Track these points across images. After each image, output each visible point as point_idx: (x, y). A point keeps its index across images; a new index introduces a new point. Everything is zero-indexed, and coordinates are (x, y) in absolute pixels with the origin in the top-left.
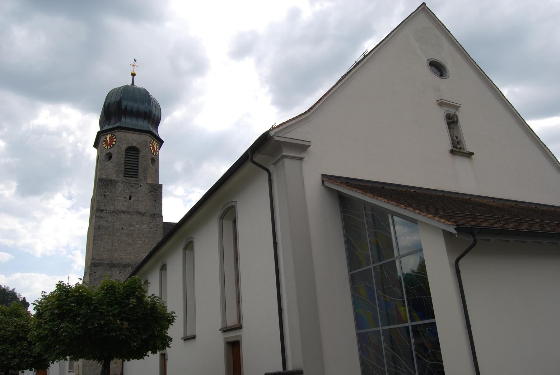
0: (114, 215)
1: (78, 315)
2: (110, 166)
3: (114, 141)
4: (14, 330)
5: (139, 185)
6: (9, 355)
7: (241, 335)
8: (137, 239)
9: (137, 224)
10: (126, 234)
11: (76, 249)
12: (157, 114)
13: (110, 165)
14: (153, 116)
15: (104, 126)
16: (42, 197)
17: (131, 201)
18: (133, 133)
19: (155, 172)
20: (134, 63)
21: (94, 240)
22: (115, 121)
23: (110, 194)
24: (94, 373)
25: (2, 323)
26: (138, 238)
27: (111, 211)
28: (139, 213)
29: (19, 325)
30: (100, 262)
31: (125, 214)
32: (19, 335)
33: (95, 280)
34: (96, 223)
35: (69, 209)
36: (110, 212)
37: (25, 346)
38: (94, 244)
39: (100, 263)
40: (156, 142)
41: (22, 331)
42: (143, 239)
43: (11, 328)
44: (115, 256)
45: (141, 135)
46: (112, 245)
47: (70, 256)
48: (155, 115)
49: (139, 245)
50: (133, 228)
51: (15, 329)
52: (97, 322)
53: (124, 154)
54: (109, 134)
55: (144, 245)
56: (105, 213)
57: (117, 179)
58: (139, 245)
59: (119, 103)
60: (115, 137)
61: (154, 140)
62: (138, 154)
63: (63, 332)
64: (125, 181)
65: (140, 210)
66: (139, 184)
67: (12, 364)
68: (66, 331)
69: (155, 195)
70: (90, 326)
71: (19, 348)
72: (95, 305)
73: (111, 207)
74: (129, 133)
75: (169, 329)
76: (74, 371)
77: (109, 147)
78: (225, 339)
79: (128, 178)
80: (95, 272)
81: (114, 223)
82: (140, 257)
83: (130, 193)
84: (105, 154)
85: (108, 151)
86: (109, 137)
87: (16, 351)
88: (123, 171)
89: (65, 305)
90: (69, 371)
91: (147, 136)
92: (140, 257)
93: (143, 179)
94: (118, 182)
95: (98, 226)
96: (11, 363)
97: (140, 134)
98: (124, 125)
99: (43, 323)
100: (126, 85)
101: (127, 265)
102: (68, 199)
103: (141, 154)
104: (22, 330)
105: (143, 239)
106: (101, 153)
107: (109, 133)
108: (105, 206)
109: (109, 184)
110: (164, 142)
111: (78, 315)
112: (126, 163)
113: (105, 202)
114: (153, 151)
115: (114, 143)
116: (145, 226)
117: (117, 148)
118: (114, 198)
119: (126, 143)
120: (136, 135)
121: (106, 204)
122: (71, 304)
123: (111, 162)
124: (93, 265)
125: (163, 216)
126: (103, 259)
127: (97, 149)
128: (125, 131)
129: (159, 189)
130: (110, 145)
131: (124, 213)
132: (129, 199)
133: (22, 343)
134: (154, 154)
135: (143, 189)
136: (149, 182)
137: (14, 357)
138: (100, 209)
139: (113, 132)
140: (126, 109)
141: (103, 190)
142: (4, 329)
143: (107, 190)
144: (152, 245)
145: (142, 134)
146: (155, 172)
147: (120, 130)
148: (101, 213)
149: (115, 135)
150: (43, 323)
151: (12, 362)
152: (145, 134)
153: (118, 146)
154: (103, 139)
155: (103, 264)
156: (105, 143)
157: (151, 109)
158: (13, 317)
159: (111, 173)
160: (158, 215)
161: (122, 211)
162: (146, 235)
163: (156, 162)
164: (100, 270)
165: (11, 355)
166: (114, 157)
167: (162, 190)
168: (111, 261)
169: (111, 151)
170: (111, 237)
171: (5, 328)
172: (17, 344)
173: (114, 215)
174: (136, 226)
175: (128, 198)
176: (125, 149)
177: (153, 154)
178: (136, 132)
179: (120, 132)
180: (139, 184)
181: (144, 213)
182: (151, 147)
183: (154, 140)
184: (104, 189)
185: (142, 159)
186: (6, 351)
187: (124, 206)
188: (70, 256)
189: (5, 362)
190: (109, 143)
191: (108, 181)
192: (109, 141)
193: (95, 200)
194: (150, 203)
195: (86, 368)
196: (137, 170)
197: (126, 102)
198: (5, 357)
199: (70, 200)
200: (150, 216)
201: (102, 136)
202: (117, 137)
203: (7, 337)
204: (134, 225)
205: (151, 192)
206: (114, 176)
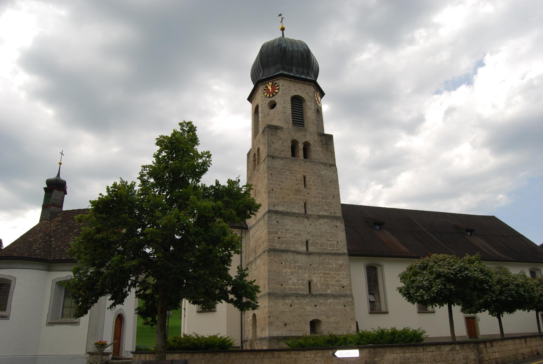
60: (277, 85)
75: (229, 271)
77: (271, 95)
78: (464, 316)
110: (325, 94)
114: (317, 102)
115: (277, 91)
130: (272, 93)
139: (275, 80)
156: (266, 91)
190: (271, 91)
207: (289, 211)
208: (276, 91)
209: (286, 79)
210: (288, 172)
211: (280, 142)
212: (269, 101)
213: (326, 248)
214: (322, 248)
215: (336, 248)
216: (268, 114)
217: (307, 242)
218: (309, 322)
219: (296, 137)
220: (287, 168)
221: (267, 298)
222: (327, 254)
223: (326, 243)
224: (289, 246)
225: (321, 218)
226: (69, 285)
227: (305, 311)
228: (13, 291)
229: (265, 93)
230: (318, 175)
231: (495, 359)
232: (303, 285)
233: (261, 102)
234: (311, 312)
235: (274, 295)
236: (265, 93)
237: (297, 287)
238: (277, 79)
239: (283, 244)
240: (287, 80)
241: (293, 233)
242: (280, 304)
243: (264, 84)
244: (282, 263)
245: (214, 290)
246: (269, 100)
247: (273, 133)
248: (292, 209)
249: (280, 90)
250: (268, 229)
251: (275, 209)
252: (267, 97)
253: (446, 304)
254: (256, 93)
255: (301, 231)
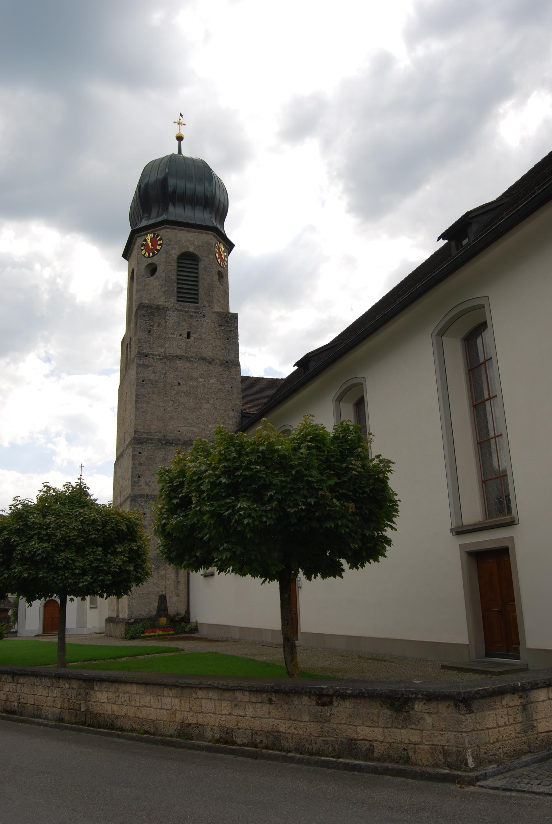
0: (165, 363)
1: (267, 487)
2: (154, 284)
3: (160, 245)
4: (81, 528)
5: (201, 315)
6: (76, 569)
7: (513, 537)
8: (203, 402)
9: (201, 377)
10: (184, 393)
11: (58, 434)
12: (222, 200)
13: (154, 282)
14: (217, 202)
15: (141, 220)
16: (8, 360)
17: (189, 340)
18: (189, 231)
19: (223, 295)
20: (180, 119)
21: (137, 402)
22: (158, 212)
23: (158, 328)
24: (146, 609)
25: (62, 516)
26: (204, 399)
27: (160, 357)
28: (203, 359)
29: (89, 520)
30: (148, 437)
31: (182, 361)
32: (89, 536)
33: (141, 464)
34: (139, 375)
35: (46, 376)
36: (158, 357)
37: (99, 555)
38: (137, 409)
39: (148, 439)
40: (224, 245)
41: (93, 531)
42: (212, 401)
43: (75, 524)
44: (170, 427)
45: (200, 235)
46: (165, 410)
47: (50, 446)
48: (220, 201)
49: (205, 411)
50: (195, 384)
51: (82, 526)
52: (303, 500)
53: (176, 264)
54: (150, 233)
55: (213, 411)
56: (151, 360)
57: (167, 305)
58: (205, 411)
59: (164, 182)
60: (160, 237)
61: (220, 243)
62: (197, 265)
63: (245, 518)
64: (179, 309)
65: (204, 355)
66: (201, 313)
67: (81, 585)
68: (249, 516)
69: (227, 331)
70: (290, 507)
71: (90, 558)
72: (298, 469)
73: (159, 349)
74: (181, 232)
76: (97, 607)
77: (151, 255)
79: (184, 303)
80: (140, 453)
81: (165, 375)
82: (208, 429)
83: (188, 328)
84: (145, 265)
85: (150, 261)
86: (151, 239)
87: (87, 563)
88: (176, 291)
89: (240, 469)
90: (92, 606)
91: (210, 236)
92: (208, 429)
93: (207, 305)
94: (169, 309)
95: (142, 380)
96: (79, 583)
97: (199, 232)
98: (173, 218)
99: (194, 502)
100: (171, 153)
101: (189, 442)
102: (45, 361)
103: (201, 266)
104: (93, 527)
105: (212, 401)
106: (137, 264)
107: (150, 231)
108: (150, 348)
109: (156, 313)
110: (234, 245)
111: (267, 487)
112: (178, 279)
113: (150, 341)
114: (219, 260)
115: (159, 247)
116: (213, 381)
117: (164, 256)
118: (164, 335)
119: (177, 247)
120: (193, 234)
121: (151, 345)
122: (253, 467)
123: (157, 278)
124: (137, 440)
125: (240, 364)
126: (152, 433)
127: (128, 260)
128: (175, 227)
129: (233, 322)
130: (152, 251)
131: (180, 359)
132: (186, 337)
133: (94, 550)
134: (222, 265)
135: (207, 321)
136: (216, 310)
137: (84, 572)
138: (144, 353)
139: (155, 231)
140: (174, 191)
141: (146, 323)
142: (65, 525)
143: (153, 322)
144: (225, 411)
145: (202, 233)
146: (223, 295)
147: (167, 226)
148: (145, 359)
149: (160, 234)
150: (194, 502)
151: (81, 580)
152: (206, 232)
153: (166, 252)
154: (139, 241)
155: (152, 439)
156: (144, 247)
157: (214, 192)
158: (75, 507)
159: (157, 296)
160: (233, 362)
161: (177, 356)
162: (215, 395)
163: (225, 278)
164: (148, 450)
165: (79, 569)
166: (160, 269)
167: (238, 322)
168: (164, 436)
169: (155, 260)
170: (162, 397)
171: (66, 524)
172: (87, 551)
173: (165, 363)
174: (200, 380)
175: (185, 335)
176: (176, 257)
177: (220, 264)
178: (194, 230)
179: (168, 230)
180: (201, 313)
181: (211, 360)
182: (217, 253)
183: (220, 243)
184: (148, 320)
185: (204, 272)
186: (70, 562)
187: (179, 348)
188: (50, 446)
189: (70, 581)
190: (151, 247)
191: (153, 308)
192: (150, 244)
193: (133, 339)
194: (219, 344)
195: (134, 601)
196: (197, 290)
197: (175, 180)
198: (70, 571)
199: (48, 364)
200: (221, 364)
201: (138, 237)
202: (163, 238)
203: (71, 538)
204: (197, 379)
205: (220, 326)
206: (162, 300)
208: (157, 248)
226: (161, 512)
229: (143, 250)
231: (548, 732)
236: (143, 250)
245: (211, 543)
252: (145, 257)
253: (15, 594)
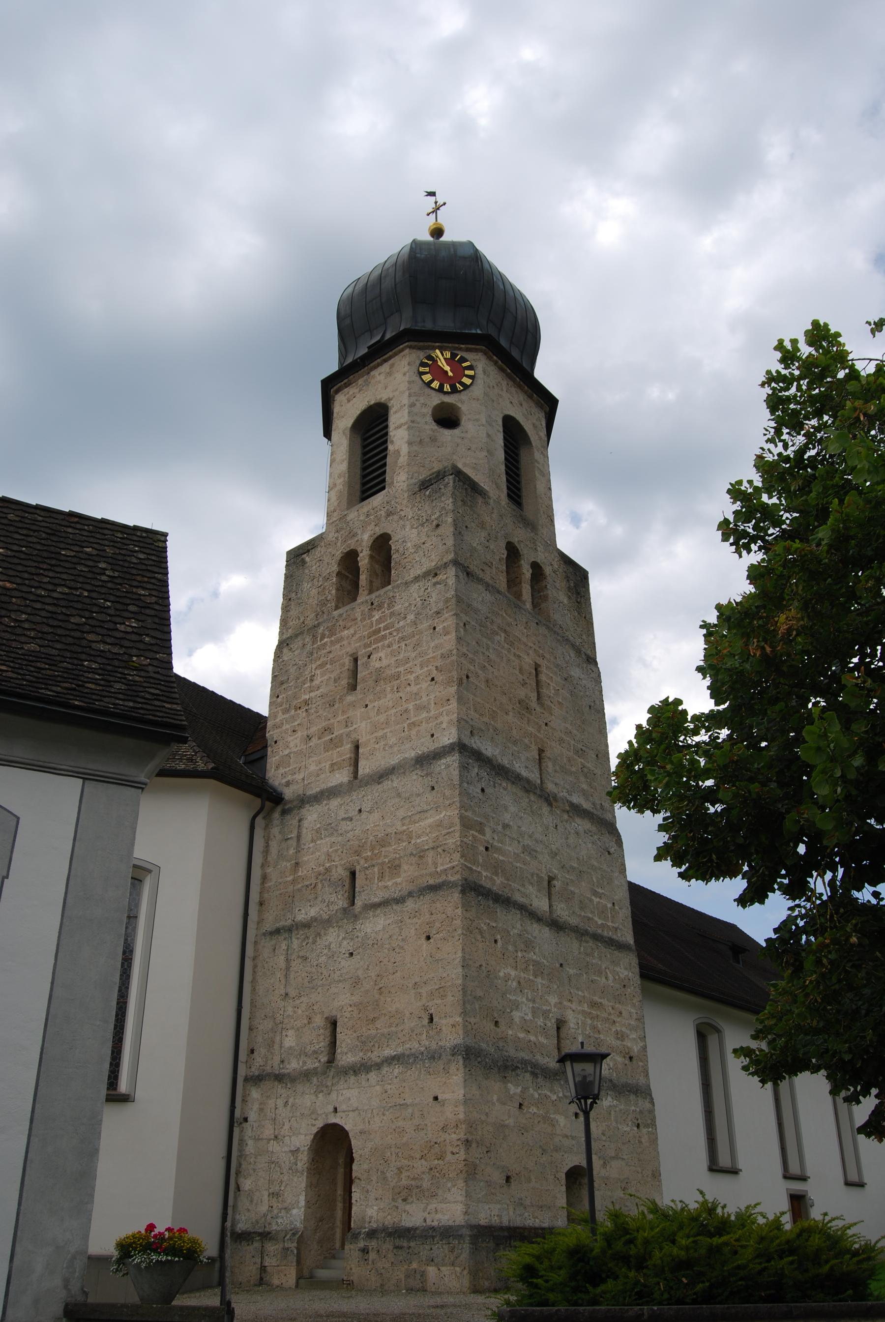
190: (450, 374)
207: (505, 762)
209: (495, 358)
210: (503, 635)
211: (483, 534)
212: (439, 402)
213: (590, 916)
214: (583, 914)
215: (612, 922)
216: (433, 440)
217: (550, 880)
218: (564, 1176)
219: (516, 540)
220: (499, 621)
221: (461, 1062)
222: (596, 937)
223: (591, 900)
224: (510, 883)
225: (578, 816)
227: (554, 1132)
228: (62, 916)
230: (566, 675)
232: (544, 1030)
233: (410, 395)
234: (567, 1136)
235: (479, 1059)
236: (426, 373)
237: (533, 1038)
238: (470, 346)
239: (497, 874)
240: (496, 363)
241: (519, 842)
242: (495, 1098)
243: (420, 348)
244: (496, 941)
246: (436, 399)
247: (466, 497)
248: (514, 762)
249: (479, 381)
250: (462, 807)
251: (474, 746)
252: (432, 388)
254: (375, 367)
255: (537, 841)
